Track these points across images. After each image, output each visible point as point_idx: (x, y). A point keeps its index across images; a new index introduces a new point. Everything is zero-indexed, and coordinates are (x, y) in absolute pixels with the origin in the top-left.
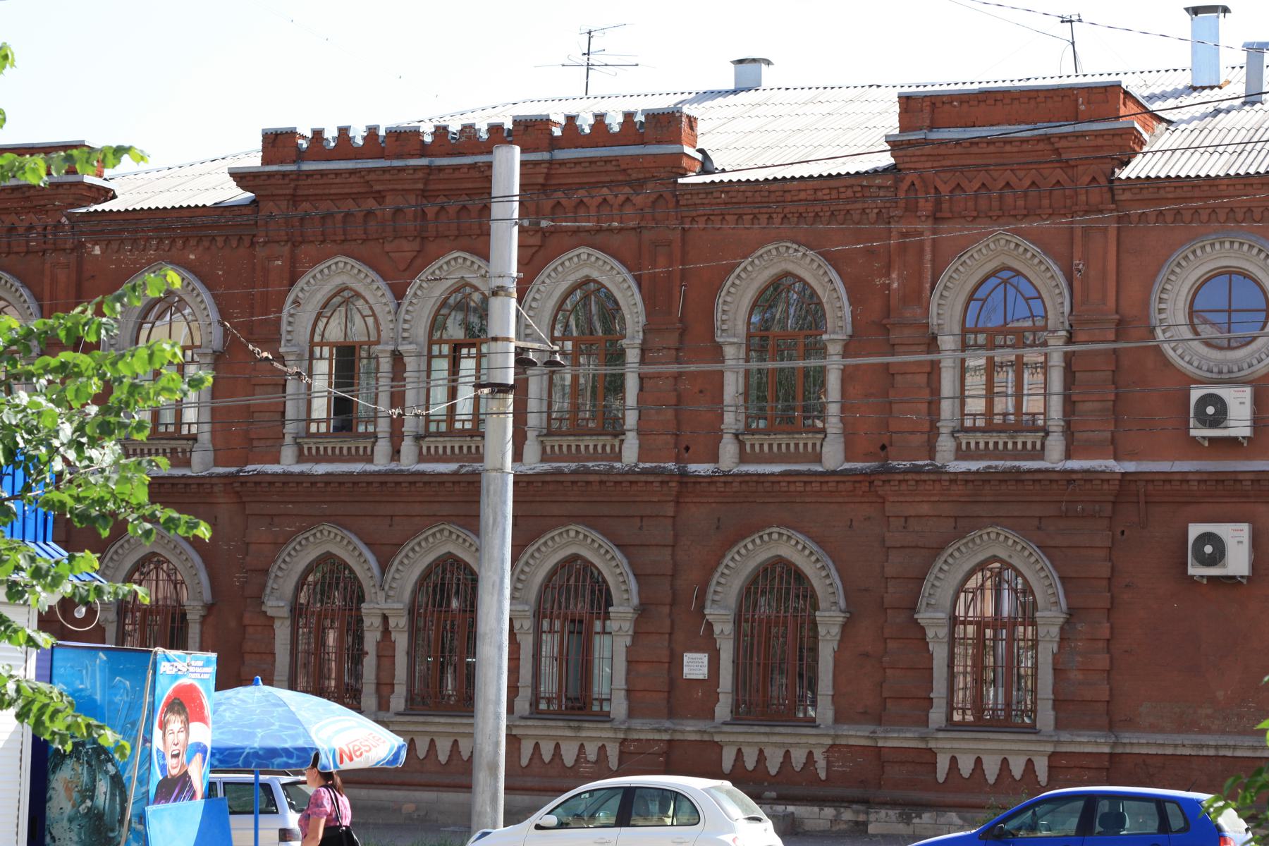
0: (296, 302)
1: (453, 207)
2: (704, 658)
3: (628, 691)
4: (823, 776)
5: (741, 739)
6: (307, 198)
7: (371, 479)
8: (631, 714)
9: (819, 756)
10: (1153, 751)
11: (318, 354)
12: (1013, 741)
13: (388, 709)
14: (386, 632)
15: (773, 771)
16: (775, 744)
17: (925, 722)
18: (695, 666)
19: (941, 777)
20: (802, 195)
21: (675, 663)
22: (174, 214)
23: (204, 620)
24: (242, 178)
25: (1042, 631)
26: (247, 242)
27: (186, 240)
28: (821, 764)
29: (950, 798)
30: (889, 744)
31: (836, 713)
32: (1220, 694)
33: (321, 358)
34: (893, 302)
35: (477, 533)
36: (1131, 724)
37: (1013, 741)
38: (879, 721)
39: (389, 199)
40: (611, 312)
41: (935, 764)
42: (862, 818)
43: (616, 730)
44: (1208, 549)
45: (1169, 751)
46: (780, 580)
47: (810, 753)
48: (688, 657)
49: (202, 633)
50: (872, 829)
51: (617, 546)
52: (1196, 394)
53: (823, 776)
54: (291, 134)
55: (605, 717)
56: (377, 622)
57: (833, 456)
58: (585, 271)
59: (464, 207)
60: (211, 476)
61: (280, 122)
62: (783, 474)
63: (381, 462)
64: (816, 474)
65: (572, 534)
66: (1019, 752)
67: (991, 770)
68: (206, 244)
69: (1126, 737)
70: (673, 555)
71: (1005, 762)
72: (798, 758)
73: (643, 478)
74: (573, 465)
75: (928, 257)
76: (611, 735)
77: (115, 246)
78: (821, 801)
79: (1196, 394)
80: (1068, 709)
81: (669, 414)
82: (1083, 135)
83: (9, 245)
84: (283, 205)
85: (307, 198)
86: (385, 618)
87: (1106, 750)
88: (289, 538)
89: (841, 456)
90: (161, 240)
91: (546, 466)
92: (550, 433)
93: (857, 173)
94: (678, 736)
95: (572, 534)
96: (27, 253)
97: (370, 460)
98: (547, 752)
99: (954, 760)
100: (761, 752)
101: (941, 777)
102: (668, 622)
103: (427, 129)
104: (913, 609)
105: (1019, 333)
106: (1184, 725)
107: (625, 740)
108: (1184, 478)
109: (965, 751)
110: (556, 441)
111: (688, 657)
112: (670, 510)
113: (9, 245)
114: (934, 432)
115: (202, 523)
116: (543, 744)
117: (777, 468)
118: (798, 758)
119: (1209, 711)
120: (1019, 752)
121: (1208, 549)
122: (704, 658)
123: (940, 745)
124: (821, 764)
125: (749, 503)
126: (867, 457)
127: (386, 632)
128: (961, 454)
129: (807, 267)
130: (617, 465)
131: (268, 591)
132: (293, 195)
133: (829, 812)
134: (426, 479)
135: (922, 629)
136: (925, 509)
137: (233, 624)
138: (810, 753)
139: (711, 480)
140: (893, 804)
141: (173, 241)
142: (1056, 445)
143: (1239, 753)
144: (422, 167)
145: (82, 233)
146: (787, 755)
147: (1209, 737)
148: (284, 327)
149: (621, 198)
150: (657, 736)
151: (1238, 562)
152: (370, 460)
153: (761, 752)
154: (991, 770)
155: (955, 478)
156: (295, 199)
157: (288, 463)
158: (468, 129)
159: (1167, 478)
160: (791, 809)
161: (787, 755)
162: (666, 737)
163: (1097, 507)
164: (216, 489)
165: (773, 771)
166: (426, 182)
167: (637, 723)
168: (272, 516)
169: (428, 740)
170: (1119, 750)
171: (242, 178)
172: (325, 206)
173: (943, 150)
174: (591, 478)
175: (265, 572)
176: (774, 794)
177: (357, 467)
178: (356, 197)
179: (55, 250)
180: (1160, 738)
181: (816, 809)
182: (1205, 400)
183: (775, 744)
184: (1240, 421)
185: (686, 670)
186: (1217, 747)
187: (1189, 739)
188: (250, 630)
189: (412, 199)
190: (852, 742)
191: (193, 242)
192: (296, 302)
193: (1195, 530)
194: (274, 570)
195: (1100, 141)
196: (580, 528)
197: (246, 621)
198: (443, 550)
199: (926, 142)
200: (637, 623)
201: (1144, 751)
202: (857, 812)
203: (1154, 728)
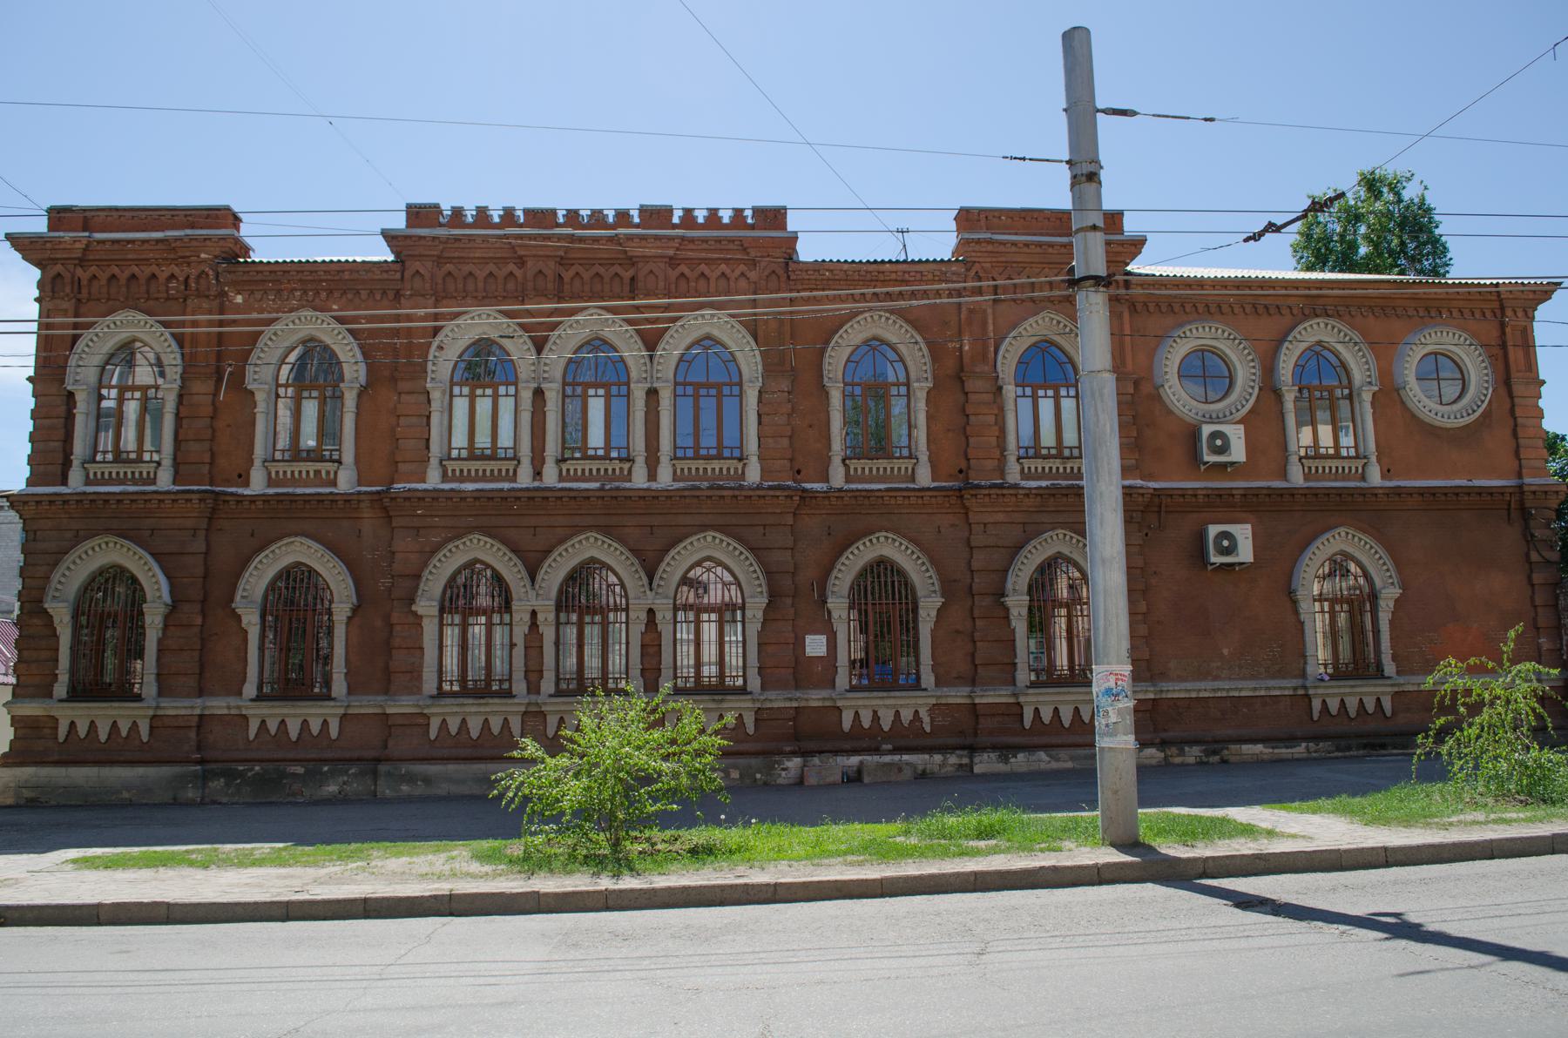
1: (104, 277)
2: (823, 638)
3: (158, 675)
4: (928, 729)
5: (875, 702)
6: (450, 260)
7: (519, 494)
8: (764, 687)
9: (923, 714)
10: (1182, 695)
13: (538, 693)
14: (534, 625)
15: (886, 728)
16: (887, 706)
17: (1013, 682)
18: (815, 645)
19: (1027, 724)
20: (893, 276)
21: (800, 644)
22: (324, 268)
24: (390, 237)
25: (516, 617)
26: (391, 295)
27: (330, 292)
28: (926, 719)
29: (1036, 740)
30: (985, 701)
31: (349, 688)
32: (1225, 651)
34: (966, 360)
35: (1083, 534)
36: (1164, 676)
38: (973, 682)
39: (530, 264)
40: (331, 362)
41: (1022, 715)
42: (965, 761)
43: (753, 700)
44: (1226, 543)
45: (1194, 695)
46: (297, 580)
47: (916, 712)
48: (809, 639)
49: (347, 633)
50: (977, 769)
51: (152, 554)
52: (1207, 430)
53: (928, 729)
54: (436, 208)
55: (138, 698)
56: (527, 618)
57: (924, 478)
58: (707, 330)
59: (133, 276)
60: (359, 493)
62: (888, 490)
63: (525, 479)
64: (914, 490)
65: (709, 539)
66: (1334, 695)
67: (294, 730)
68: (350, 296)
69: (1165, 686)
71: (1077, 710)
72: (907, 715)
73: (771, 493)
74: (597, 485)
75: (991, 328)
76: (750, 705)
77: (258, 295)
78: (930, 750)
79: (1207, 430)
81: (785, 442)
83: (148, 292)
84: (429, 264)
85: (450, 260)
86: (534, 614)
87: (1152, 696)
88: (434, 551)
90: (305, 292)
91: (677, 485)
92: (676, 458)
94: (803, 704)
95: (709, 539)
96: (168, 299)
97: (514, 479)
98: (453, 726)
100: (875, 712)
101: (1027, 724)
102: (792, 611)
103: (446, 207)
104: (412, 601)
105: (719, 386)
106: (1202, 675)
107: (154, 716)
108: (1195, 493)
109: (1044, 703)
110: (685, 465)
111: (809, 639)
112: (790, 520)
113: (148, 292)
114: (1002, 459)
116: (1062, 709)
117: (882, 486)
118: (907, 715)
120: (1334, 695)
121: (1226, 543)
122: (823, 638)
123: (252, 712)
124: (926, 719)
125: (858, 514)
126: (951, 477)
127: (534, 625)
128: (1025, 475)
129: (895, 332)
132: (439, 257)
133: (938, 758)
134: (572, 494)
135: (1007, 609)
136: (1001, 517)
137: (379, 623)
138: (916, 712)
139: (827, 495)
140: (994, 748)
141: (317, 293)
143: (1243, 694)
145: (226, 284)
146: (897, 713)
148: (430, 366)
149: (737, 273)
150: (788, 704)
151: (1245, 553)
152: (64, 482)
153: (875, 712)
154: (294, 730)
155: (1029, 493)
156: (440, 260)
157: (433, 480)
158: (458, 212)
159: (1183, 493)
161: (897, 713)
162: (795, 704)
164: (362, 505)
165: (886, 728)
167: (771, 694)
168: (418, 529)
169: (300, 721)
170: (160, 712)
171: (390, 237)
172: (467, 268)
174: (725, 493)
175: (419, 577)
176: (890, 747)
177: (506, 486)
178: (505, 260)
179: (198, 296)
180: (1189, 685)
182: (1215, 435)
183: (887, 706)
184: (1238, 453)
185: (808, 650)
188: (398, 628)
189: (552, 264)
190: (951, 701)
191: (336, 294)
192: (440, 348)
193: (1213, 530)
194: (426, 573)
195: (1120, 249)
196: (717, 535)
197: (394, 620)
198: (587, 555)
199: (990, 242)
200: (765, 612)
201: (1176, 695)
202: (960, 757)
203: (1181, 679)
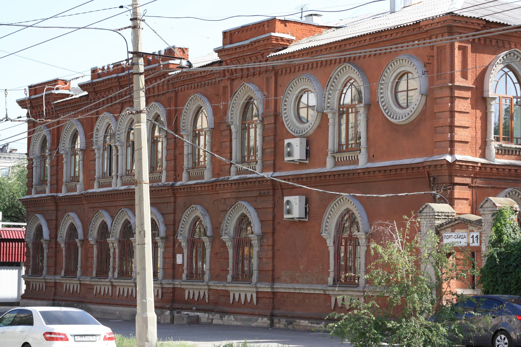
0: (97, 129)
11: (251, 127)
12: (247, 287)
21: (174, 258)
23: (82, 245)
33: (252, 128)
37: (247, 287)
61: (94, 66)
70: (174, 217)
80: (212, 278)
82: (259, 41)
89: (210, 176)
93: (471, 17)
99: (234, 294)
115: (69, 213)
119: (299, 274)
130: (160, 184)
131: (89, 235)
142: (258, 167)
144: (115, 78)
147: (297, 285)
160: (198, 314)
163: (266, 192)
166: (119, 83)
173: (230, 52)
181: (204, 314)
186: (300, 289)
187: (297, 286)
203: (286, 282)
